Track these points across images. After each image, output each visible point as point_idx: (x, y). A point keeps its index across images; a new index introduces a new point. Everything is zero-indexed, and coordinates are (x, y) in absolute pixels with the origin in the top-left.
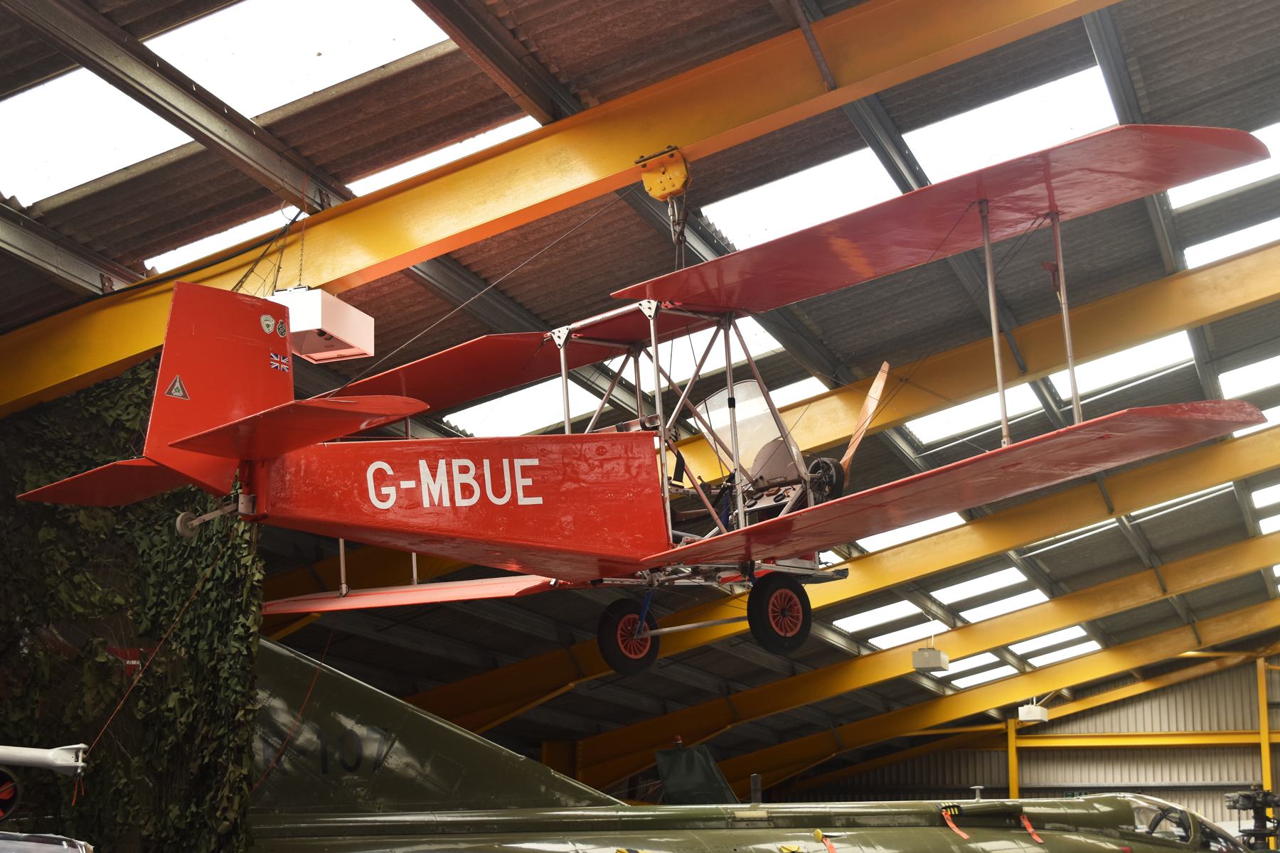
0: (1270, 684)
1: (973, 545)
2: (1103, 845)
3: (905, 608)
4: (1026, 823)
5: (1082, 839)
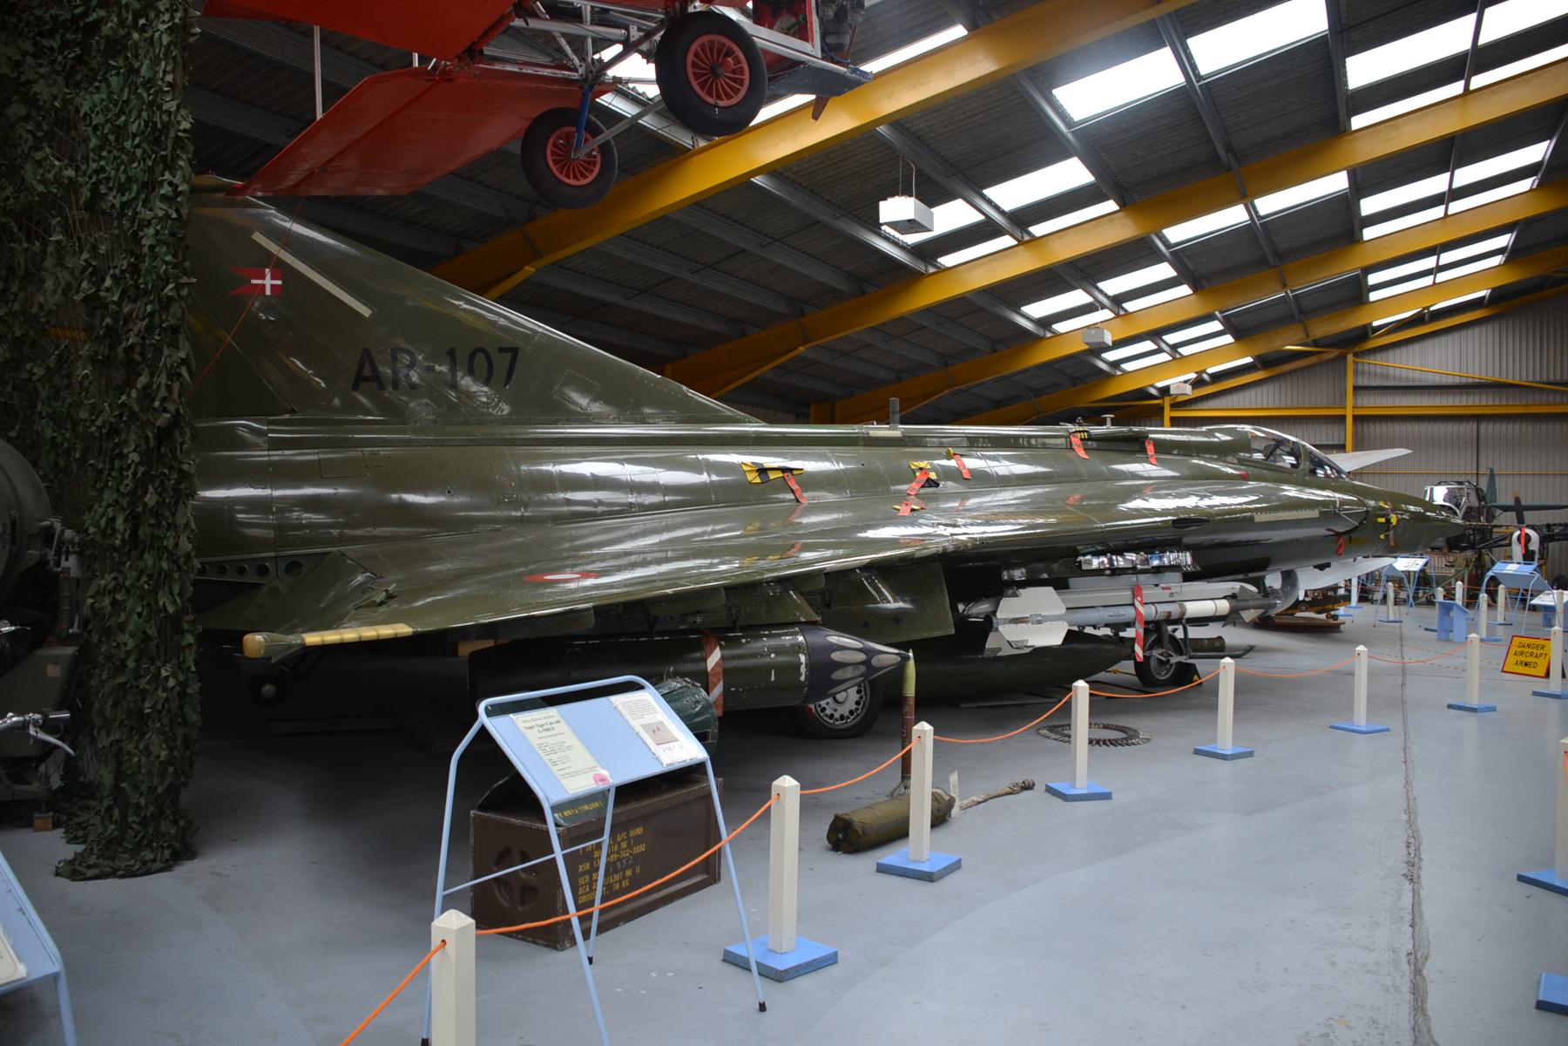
0: (1356, 372)
1: (1124, 231)
3: (1148, 345)
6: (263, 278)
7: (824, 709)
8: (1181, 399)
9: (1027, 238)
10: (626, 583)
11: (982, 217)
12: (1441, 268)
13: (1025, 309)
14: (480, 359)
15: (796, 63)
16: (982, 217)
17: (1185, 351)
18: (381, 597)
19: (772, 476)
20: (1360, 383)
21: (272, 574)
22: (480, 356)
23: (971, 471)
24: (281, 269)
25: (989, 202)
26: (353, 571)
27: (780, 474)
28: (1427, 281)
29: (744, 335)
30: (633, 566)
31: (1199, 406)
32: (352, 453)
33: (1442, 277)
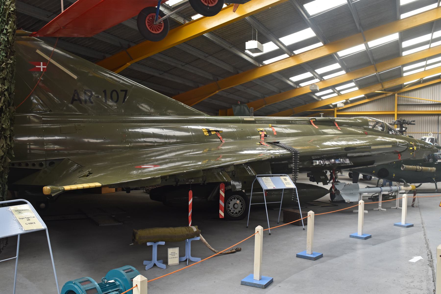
0: (398, 100)
1: (325, 52)
3: (330, 91)
4: (336, 124)
5: (353, 130)
6: (43, 66)
7: (230, 211)
8: (340, 108)
9: (292, 55)
10: (170, 168)
11: (278, 48)
12: (427, 65)
13: (291, 79)
14: (114, 94)
16: (278, 48)
17: (342, 93)
19: (213, 133)
20: (400, 104)
21: (44, 166)
22: (114, 93)
24: (45, 62)
25: (281, 43)
26: (72, 165)
27: (215, 133)
28: (423, 69)
29: (198, 87)
30: (166, 163)
31: (346, 111)
32: (68, 125)
33: (427, 68)
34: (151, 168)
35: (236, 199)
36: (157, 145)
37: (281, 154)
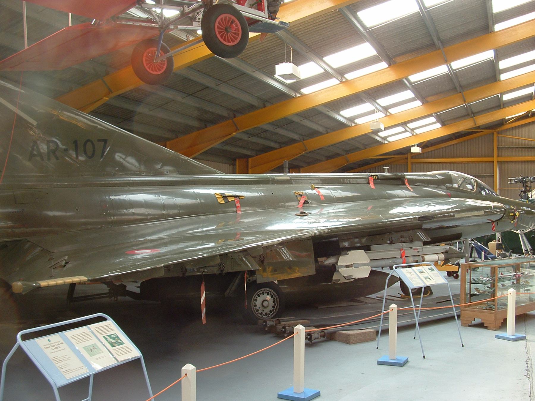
1: (390, 77)
2: (439, 192)
3: (400, 129)
7: (258, 311)
9: (344, 80)
15: (257, 21)
18: (63, 263)
23: (324, 196)
30: (165, 244)
34: (143, 254)
35: (266, 294)
36: (151, 219)
37: (329, 229)
